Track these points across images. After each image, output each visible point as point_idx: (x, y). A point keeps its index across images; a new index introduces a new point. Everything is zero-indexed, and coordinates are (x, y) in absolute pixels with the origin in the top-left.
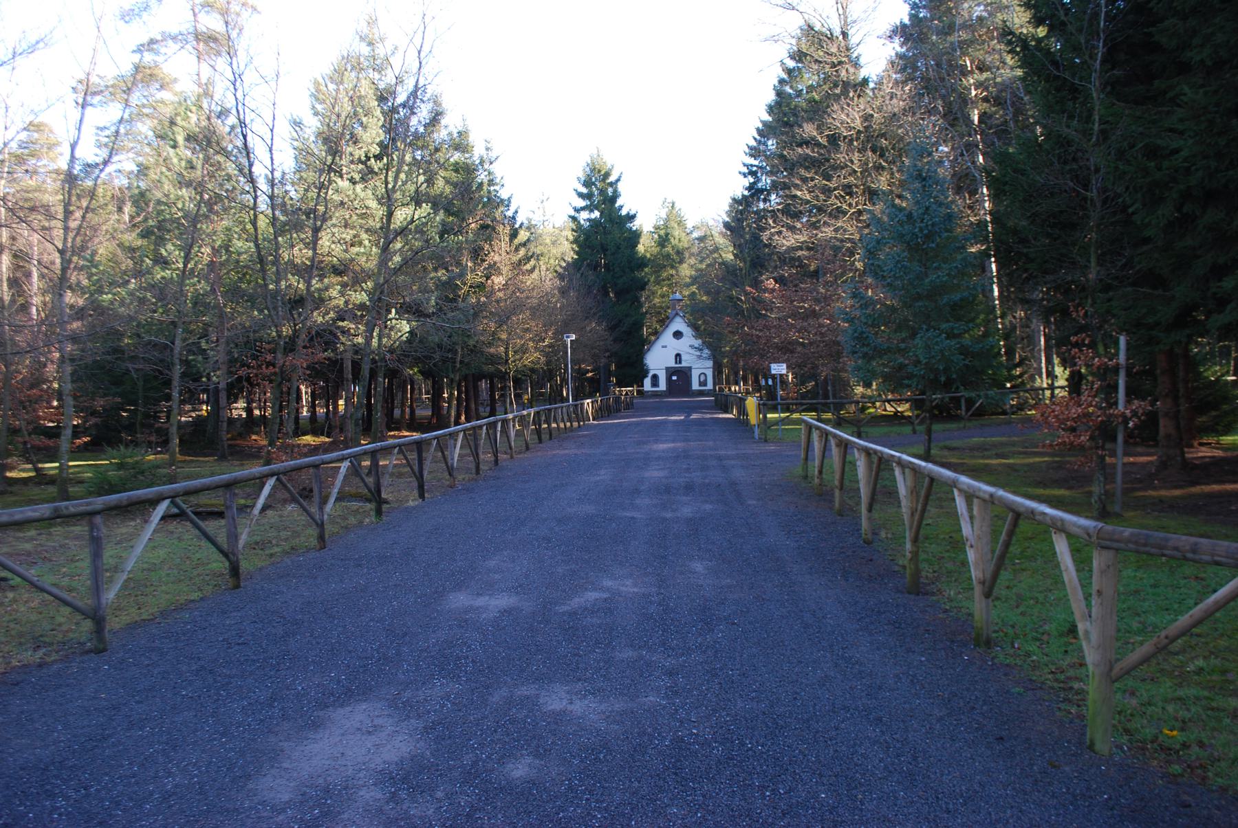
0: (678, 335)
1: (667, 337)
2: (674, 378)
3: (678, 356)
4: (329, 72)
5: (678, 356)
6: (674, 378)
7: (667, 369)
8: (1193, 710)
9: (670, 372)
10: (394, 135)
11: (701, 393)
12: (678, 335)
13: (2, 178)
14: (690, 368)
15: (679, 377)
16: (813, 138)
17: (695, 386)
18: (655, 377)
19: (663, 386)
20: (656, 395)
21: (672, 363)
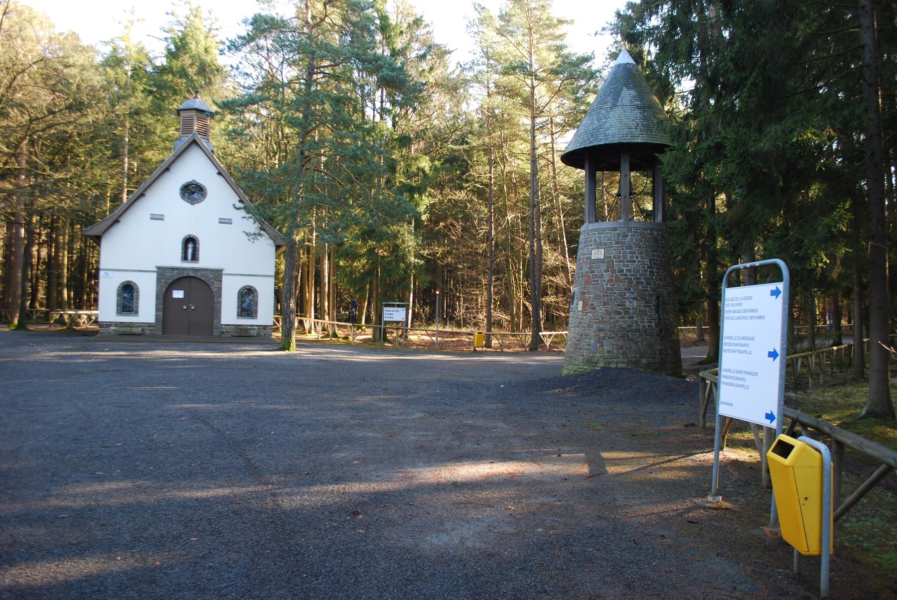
0: (193, 192)
1: (166, 195)
2: (178, 294)
3: (190, 242)
4: (146, 48)
5: (190, 242)
6: (178, 294)
7: (162, 272)
8: (73, 170)
9: (169, 280)
10: (75, 36)
11: (242, 336)
12: (193, 192)
13: (634, 599)
14: (218, 274)
15: (189, 294)
16: (553, 275)
17: (229, 315)
18: (128, 292)
19: (147, 311)
20: (129, 335)
21: (174, 259)
